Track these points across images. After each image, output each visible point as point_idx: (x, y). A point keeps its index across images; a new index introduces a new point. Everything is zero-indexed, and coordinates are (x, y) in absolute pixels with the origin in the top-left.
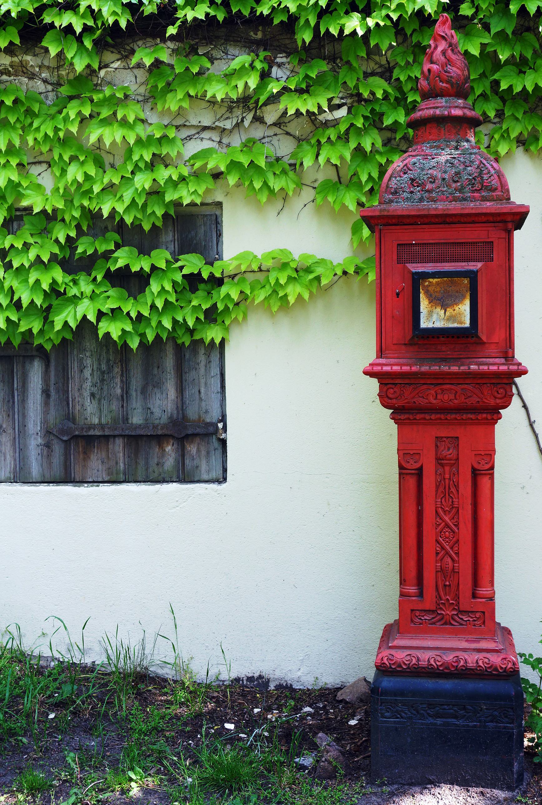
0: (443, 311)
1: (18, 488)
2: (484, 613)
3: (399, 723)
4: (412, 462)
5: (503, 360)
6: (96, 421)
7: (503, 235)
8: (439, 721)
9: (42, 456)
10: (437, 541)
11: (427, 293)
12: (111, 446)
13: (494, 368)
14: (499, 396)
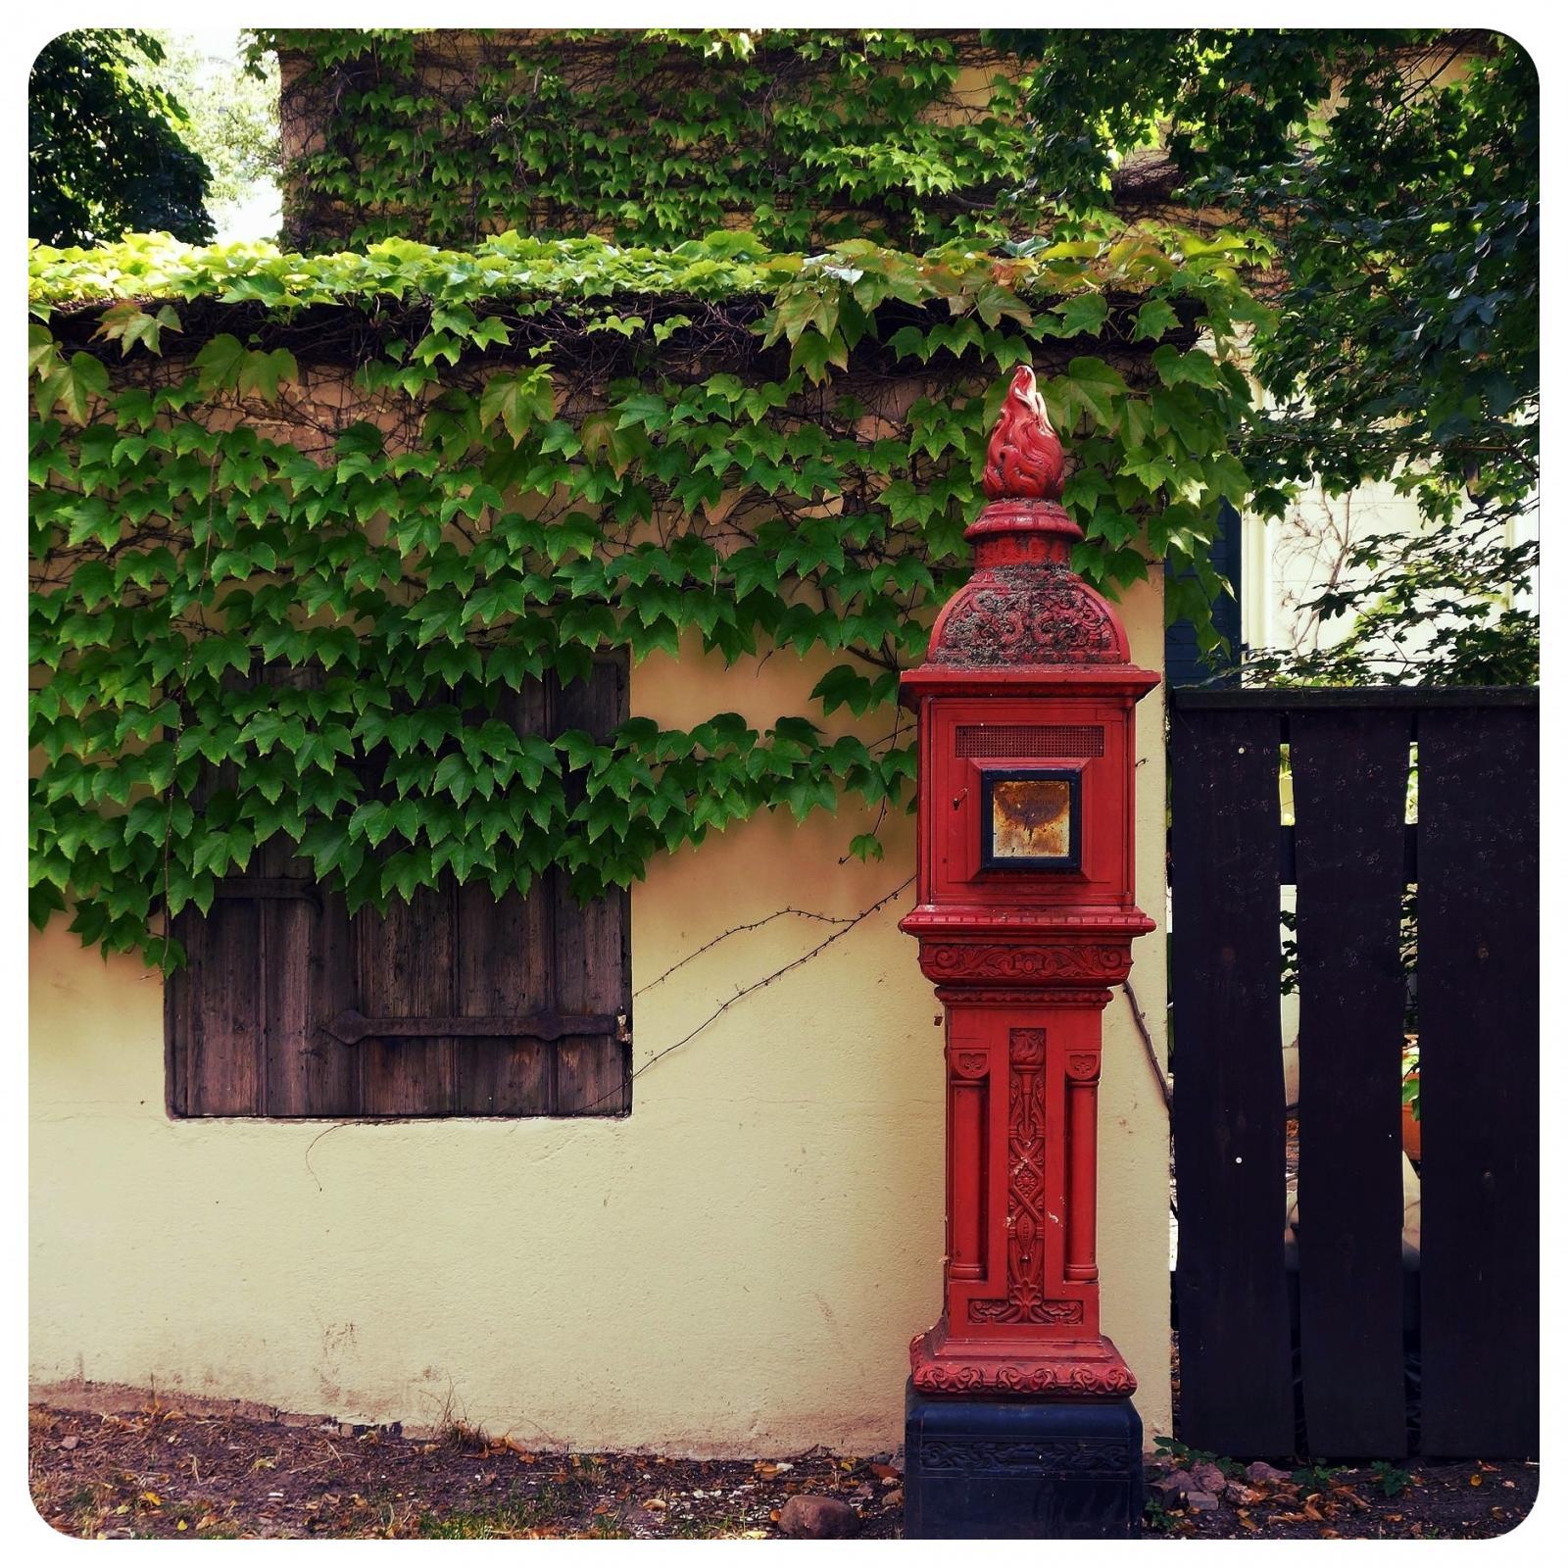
0: (1027, 832)
1: (265, 1126)
2: (1081, 1302)
3: (954, 1473)
4: (972, 1067)
5: (1118, 909)
6: (404, 1010)
7: (1119, 715)
8: (1014, 1469)
9: (308, 1071)
10: (1011, 1192)
11: (1003, 803)
12: (429, 1055)
13: (1103, 921)
14: (1110, 964)
